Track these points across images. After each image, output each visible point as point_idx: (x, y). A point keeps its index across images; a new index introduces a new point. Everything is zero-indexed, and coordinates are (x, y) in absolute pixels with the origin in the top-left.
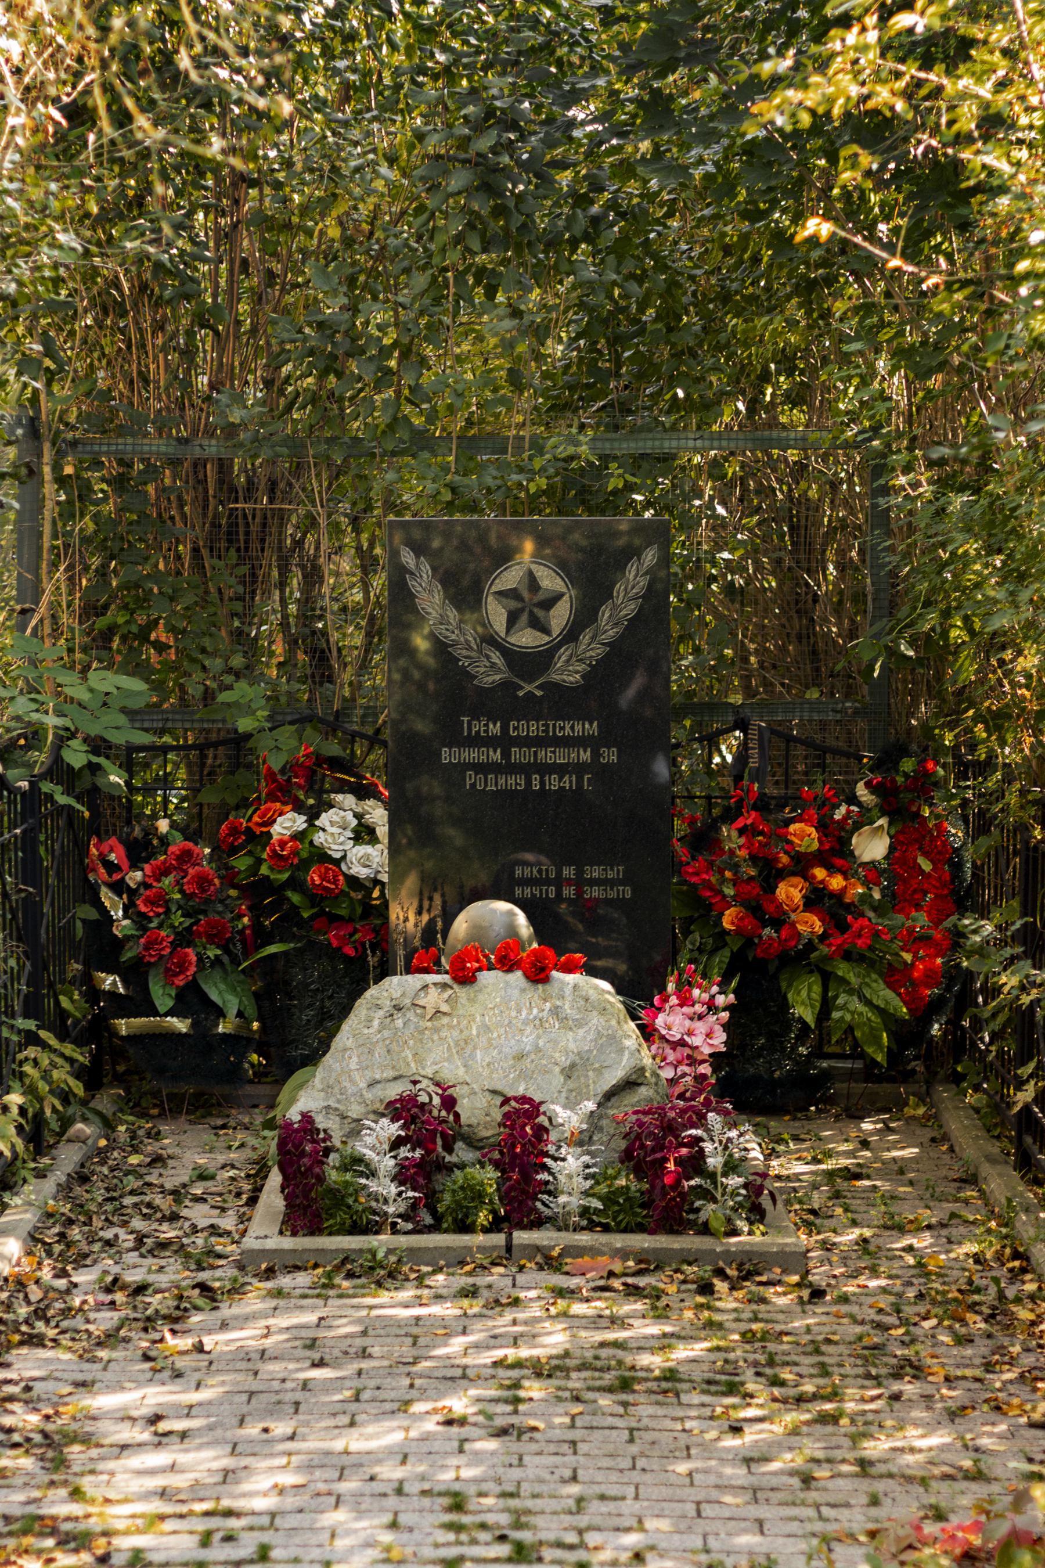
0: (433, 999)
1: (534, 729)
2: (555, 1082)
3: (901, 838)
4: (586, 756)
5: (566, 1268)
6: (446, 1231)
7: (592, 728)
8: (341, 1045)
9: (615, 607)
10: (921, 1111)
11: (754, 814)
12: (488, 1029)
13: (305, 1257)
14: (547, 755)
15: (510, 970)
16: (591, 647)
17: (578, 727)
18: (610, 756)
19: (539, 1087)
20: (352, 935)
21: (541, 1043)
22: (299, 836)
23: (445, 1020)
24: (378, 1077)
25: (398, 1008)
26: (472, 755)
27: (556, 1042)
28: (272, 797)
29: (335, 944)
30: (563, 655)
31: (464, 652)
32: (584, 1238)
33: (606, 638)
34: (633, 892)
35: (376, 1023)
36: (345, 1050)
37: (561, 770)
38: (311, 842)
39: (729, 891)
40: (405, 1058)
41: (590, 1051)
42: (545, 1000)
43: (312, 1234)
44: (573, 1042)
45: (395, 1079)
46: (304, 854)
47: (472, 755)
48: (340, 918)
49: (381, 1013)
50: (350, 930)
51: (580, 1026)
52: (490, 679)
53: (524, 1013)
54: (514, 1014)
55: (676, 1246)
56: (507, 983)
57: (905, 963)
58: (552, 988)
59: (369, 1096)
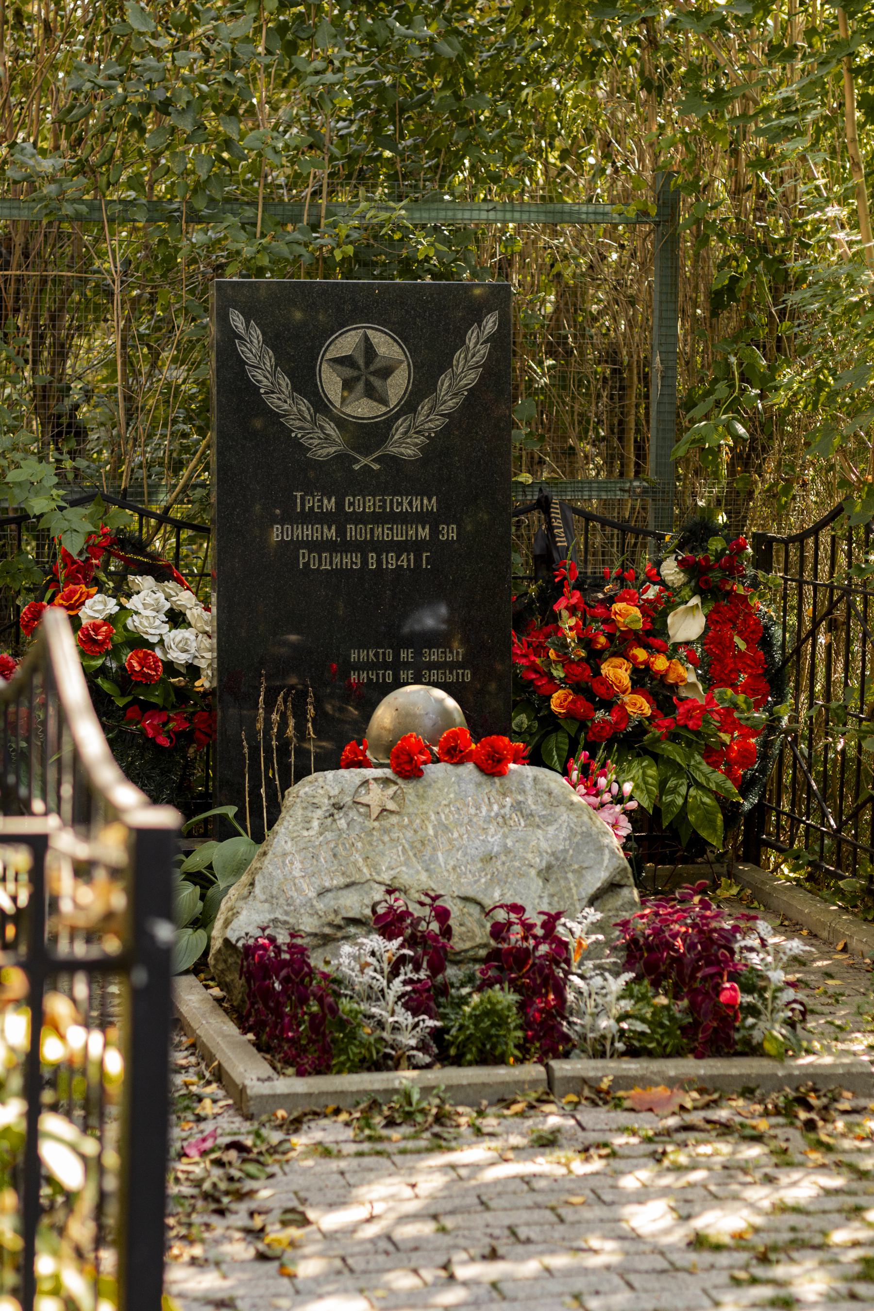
0: (375, 796)
1: (369, 504)
2: (534, 887)
3: (715, 617)
4: (424, 533)
5: (627, 1104)
6: (470, 1064)
7: (431, 504)
8: (279, 850)
9: (454, 376)
10: (734, 891)
11: (578, 594)
12: (447, 829)
13: (323, 1101)
14: (383, 533)
15: (460, 762)
16: (430, 419)
17: (417, 503)
18: (449, 533)
19: (517, 893)
20: (165, 724)
21: (510, 843)
22: (111, 620)
23: (394, 819)
24: (327, 884)
25: (338, 807)
26: (307, 532)
27: (525, 841)
28: (72, 578)
29: (151, 733)
30: (401, 426)
31: (298, 423)
32: (632, 1067)
33: (444, 409)
34: (473, 675)
35: (315, 824)
36: (285, 855)
37: (400, 548)
38: (125, 627)
39: (558, 673)
40: (355, 863)
41: (565, 851)
42: (504, 795)
43: (319, 1073)
44: (546, 840)
45: (348, 886)
46: (118, 639)
47: (307, 532)
48: (154, 706)
49: (319, 813)
50: (165, 719)
51: (549, 823)
52: (325, 452)
53: (484, 810)
54: (472, 811)
55: (734, 1071)
56: (458, 776)
57: (723, 744)
58: (510, 781)
59: (320, 906)
